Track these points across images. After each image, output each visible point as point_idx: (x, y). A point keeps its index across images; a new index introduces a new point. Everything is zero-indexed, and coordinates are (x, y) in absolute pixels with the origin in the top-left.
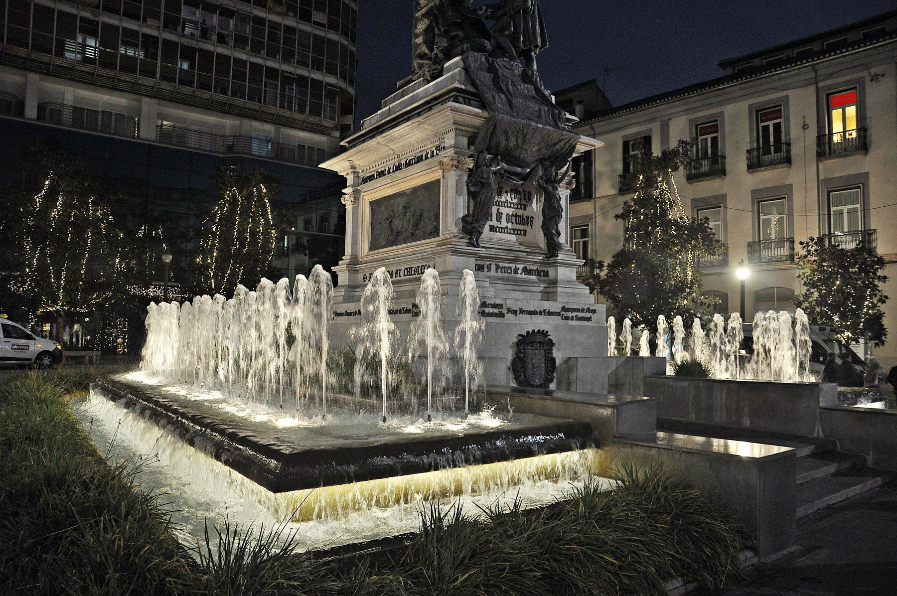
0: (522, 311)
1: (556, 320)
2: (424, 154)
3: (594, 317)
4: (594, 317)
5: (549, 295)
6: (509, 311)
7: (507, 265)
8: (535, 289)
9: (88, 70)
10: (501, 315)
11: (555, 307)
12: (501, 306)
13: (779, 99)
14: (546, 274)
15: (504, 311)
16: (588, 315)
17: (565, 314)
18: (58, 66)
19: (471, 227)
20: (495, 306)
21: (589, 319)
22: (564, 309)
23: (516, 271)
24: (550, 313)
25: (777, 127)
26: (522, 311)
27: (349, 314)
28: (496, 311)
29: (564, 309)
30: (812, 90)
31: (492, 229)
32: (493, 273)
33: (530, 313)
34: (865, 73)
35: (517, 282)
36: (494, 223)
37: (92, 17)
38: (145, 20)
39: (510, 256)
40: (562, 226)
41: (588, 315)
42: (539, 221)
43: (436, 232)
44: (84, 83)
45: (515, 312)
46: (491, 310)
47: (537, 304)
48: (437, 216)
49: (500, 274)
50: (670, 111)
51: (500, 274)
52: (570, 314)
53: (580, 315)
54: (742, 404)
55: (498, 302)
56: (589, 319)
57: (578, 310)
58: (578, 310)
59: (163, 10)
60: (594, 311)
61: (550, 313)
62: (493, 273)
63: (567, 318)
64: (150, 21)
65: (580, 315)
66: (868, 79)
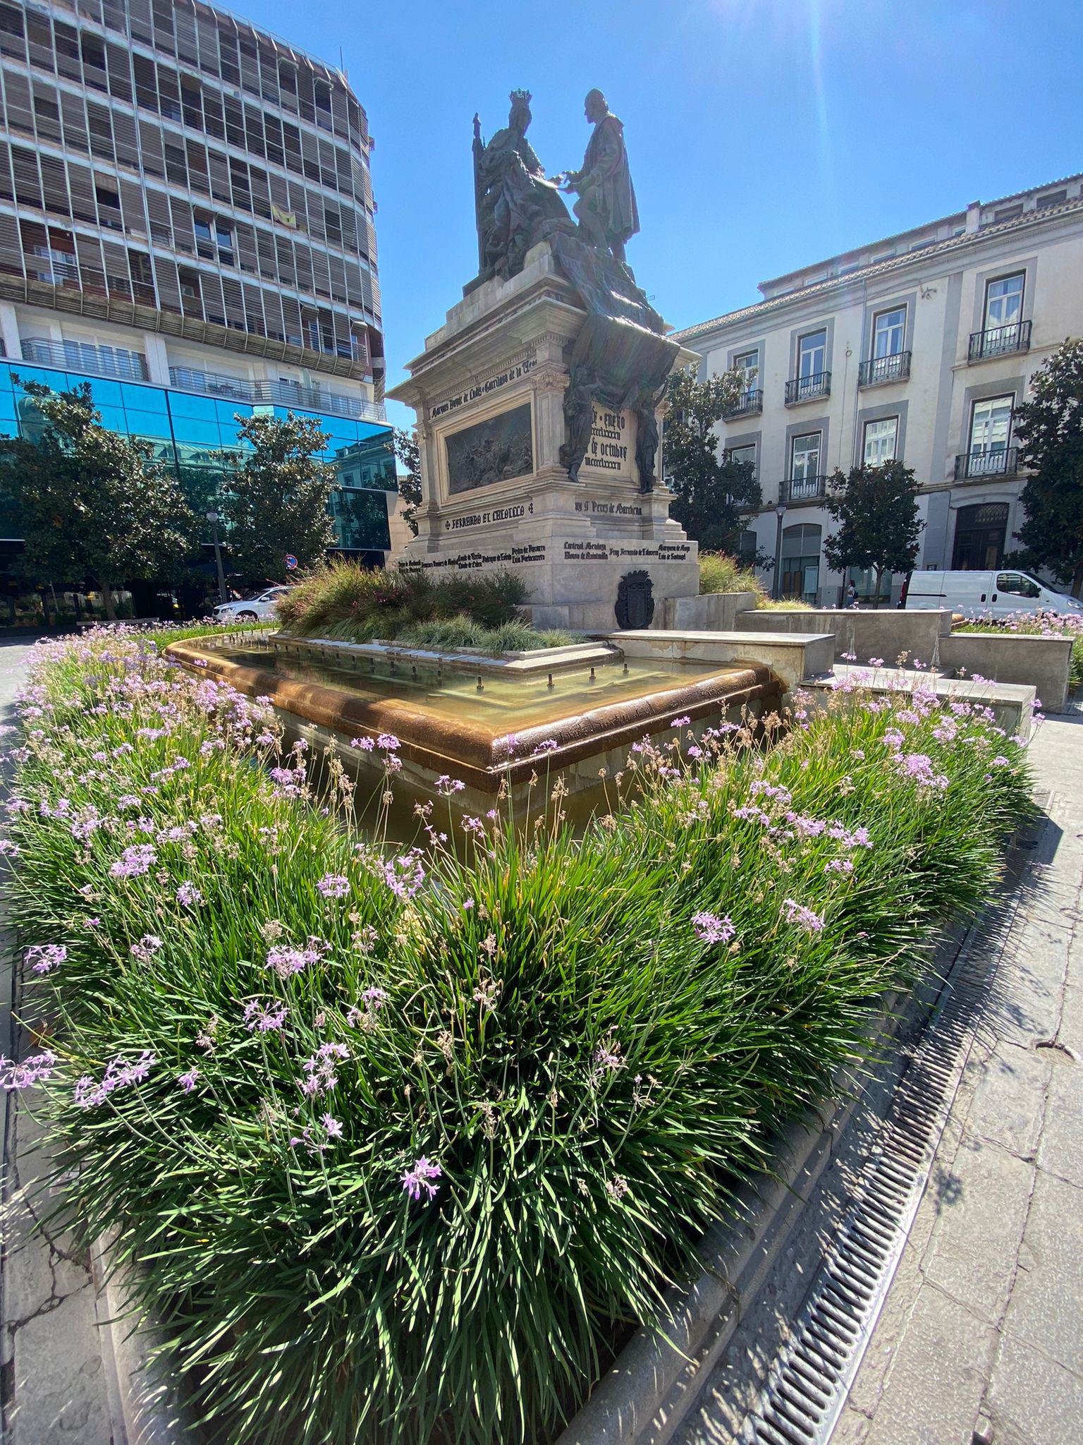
0: (623, 552)
1: (655, 558)
2: (508, 373)
3: (688, 554)
4: (688, 554)
5: (646, 535)
6: (612, 551)
7: (603, 503)
8: (630, 528)
9: (71, 296)
10: (604, 556)
11: (652, 545)
12: (604, 547)
13: (823, 322)
14: (639, 512)
15: (607, 553)
16: (681, 553)
17: (662, 553)
18: (34, 291)
19: (570, 458)
20: (598, 547)
21: (683, 557)
22: (661, 548)
23: (612, 508)
24: (649, 553)
25: (819, 355)
26: (623, 552)
27: (439, 564)
28: (600, 552)
29: (661, 548)
30: (861, 308)
32: (590, 512)
33: (630, 553)
34: (917, 289)
35: (617, 521)
37: (63, 228)
38: (128, 232)
39: (607, 493)
40: (658, 457)
41: (681, 553)
42: (631, 453)
43: (528, 468)
44: (69, 312)
45: (617, 553)
46: (593, 552)
47: (634, 544)
48: (529, 449)
49: (596, 513)
50: (960, 263)
51: (596, 513)
52: (666, 553)
53: (676, 553)
54: (848, 635)
55: (601, 542)
56: (683, 557)
57: (674, 548)
58: (674, 548)
59: (147, 219)
60: (688, 549)
61: (649, 553)
62: (590, 512)
63: (664, 557)
64: (134, 233)
65: (579, 552)
66: (919, 295)
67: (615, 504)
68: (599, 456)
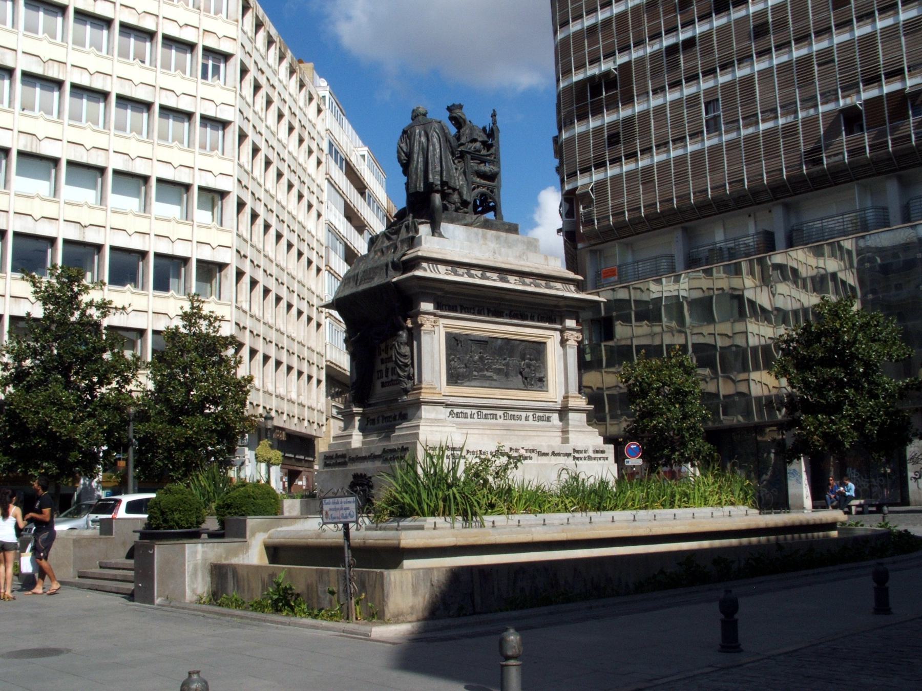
7: (389, 415)
31: (383, 385)
36: (384, 379)
67: (397, 413)
68: (390, 377)
